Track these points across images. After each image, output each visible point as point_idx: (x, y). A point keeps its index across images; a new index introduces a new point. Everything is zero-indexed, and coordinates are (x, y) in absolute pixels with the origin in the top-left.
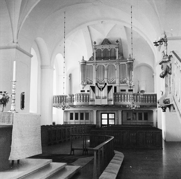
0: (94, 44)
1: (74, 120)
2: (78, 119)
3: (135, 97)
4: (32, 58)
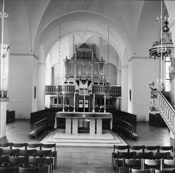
0: (75, 47)
1: (57, 104)
2: (61, 103)
3: (106, 89)
4: (151, 111)
